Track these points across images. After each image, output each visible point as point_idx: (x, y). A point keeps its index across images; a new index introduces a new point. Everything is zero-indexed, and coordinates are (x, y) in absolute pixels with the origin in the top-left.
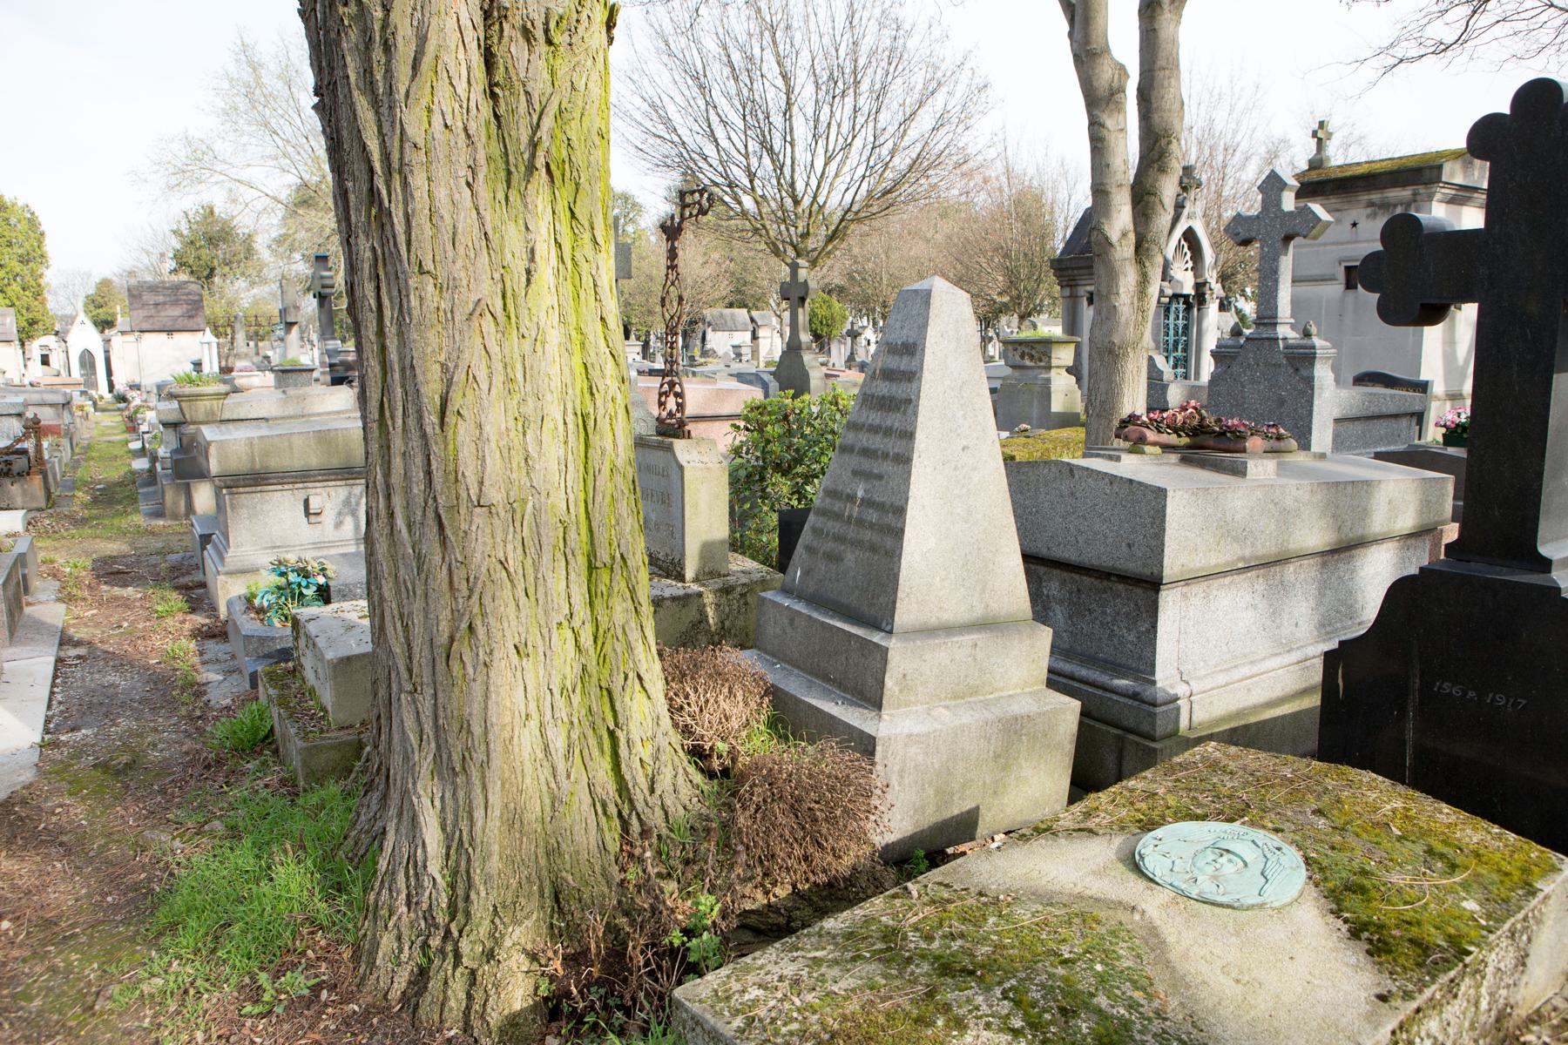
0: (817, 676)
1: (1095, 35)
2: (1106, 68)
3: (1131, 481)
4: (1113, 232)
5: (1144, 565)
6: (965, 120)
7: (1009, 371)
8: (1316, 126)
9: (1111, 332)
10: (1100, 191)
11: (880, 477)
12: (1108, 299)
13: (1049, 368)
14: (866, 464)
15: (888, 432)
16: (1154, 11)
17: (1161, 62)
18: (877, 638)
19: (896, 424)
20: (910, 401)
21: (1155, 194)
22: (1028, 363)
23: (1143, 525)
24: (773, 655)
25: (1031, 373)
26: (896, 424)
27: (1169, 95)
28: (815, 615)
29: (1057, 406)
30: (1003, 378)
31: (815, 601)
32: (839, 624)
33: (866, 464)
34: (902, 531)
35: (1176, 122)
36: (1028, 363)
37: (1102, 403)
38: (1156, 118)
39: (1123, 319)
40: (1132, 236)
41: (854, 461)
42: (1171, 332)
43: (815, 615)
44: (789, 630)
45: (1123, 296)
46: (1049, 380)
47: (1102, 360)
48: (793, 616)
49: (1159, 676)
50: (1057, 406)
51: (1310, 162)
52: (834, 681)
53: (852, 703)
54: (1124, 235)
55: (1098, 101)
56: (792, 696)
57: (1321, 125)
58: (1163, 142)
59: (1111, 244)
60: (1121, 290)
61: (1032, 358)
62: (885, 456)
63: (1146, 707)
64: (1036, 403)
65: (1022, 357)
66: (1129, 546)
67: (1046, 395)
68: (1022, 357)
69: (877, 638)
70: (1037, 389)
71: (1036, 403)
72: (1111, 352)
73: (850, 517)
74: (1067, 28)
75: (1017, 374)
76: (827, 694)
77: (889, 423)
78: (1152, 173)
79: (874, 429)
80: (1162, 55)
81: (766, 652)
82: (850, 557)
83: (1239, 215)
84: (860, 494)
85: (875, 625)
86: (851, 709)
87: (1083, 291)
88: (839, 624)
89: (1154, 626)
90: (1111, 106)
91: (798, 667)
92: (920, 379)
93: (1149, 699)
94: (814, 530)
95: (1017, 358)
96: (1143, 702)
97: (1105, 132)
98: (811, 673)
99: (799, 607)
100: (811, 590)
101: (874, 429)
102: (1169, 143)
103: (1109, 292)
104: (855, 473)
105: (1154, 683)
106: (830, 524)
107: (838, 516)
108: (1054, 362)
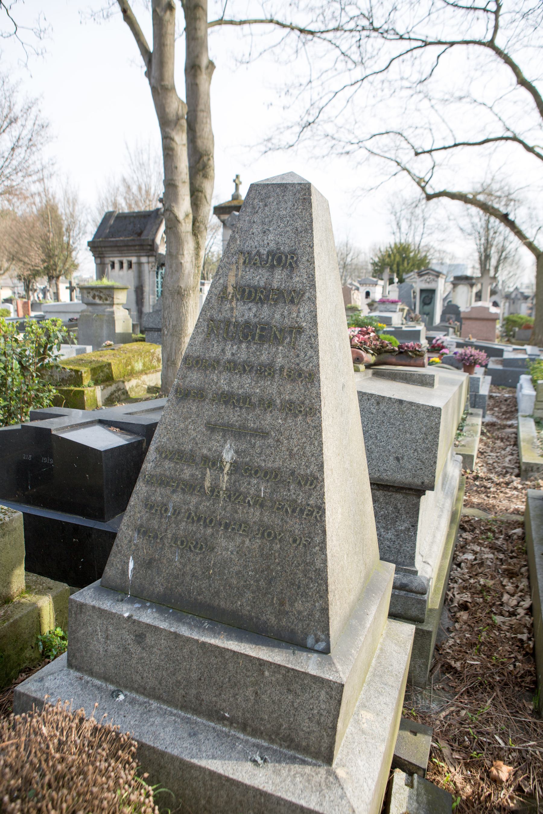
0: (196, 711)
1: (167, 75)
2: (174, 100)
3: (401, 402)
4: (181, 216)
5: (414, 476)
6: (31, 145)
7: (84, 307)
8: (235, 178)
9: (178, 280)
10: (170, 184)
11: (263, 434)
12: (177, 258)
13: (112, 305)
14: (233, 416)
15: (265, 371)
16: (196, 71)
17: (201, 107)
18: (310, 664)
19: (279, 361)
20: (300, 330)
21: (202, 192)
22: (97, 301)
23: (415, 441)
24: (106, 679)
25: (99, 308)
26: (279, 361)
27: (207, 130)
28: (185, 631)
29: (119, 329)
30: (82, 312)
31: (165, 603)
32: (233, 645)
33: (233, 416)
34: (321, 509)
35: (211, 147)
36: (97, 301)
37: (174, 326)
38: (199, 142)
39: (186, 272)
40: (191, 216)
41: (210, 411)
42: (160, 286)
43: (185, 631)
44: (134, 648)
45: (186, 256)
46: (113, 313)
47: (173, 298)
48: (141, 633)
49: (418, 565)
50: (119, 329)
51: (233, 196)
52: (231, 722)
53: (280, 758)
54: (187, 216)
55: (165, 122)
56: (173, 759)
57: (237, 176)
58: (205, 158)
59: (179, 221)
60: (185, 253)
61: (100, 298)
62: (267, 404)
63: (413, 595)
64: (105, 327)
65: (94, 297)
66: (397, 459)
67: (111, 321)
68: (94, 297)
69: (310, 664)
70: (105, 318)
71: (105, 327)
72: (179, 293)
73: (215, 488)
74: (145, 69)
75: (90, 308)
76: (229, 751)
77: (264, 358)
78: (199, 178)
79: (234, 367)
80: (202, 101)
81: (91, 673)
82: (226, 546)
83: (90, 244)
84: (228, 456)
85: (295, 642)
86: (285, 769)
87: (108, 260)
88: (233, 645)
89: (414, 525)
90: (178, 127)
91: (158, 698)
92: (313, 300)
93: (419, 589)
94: (149, 505)
95: (90, 298)
96: (411, 591)
97: (174, 145)
98: (184, 707)
99: (148, 617)
100: (160, 589)
101: (234, 367)
102: (209, 159)
103: (178, 253)
104: (212, 428)
105: (416, 573)
106: (177, 498)
107: (192, 487)
108: (116, 301)
